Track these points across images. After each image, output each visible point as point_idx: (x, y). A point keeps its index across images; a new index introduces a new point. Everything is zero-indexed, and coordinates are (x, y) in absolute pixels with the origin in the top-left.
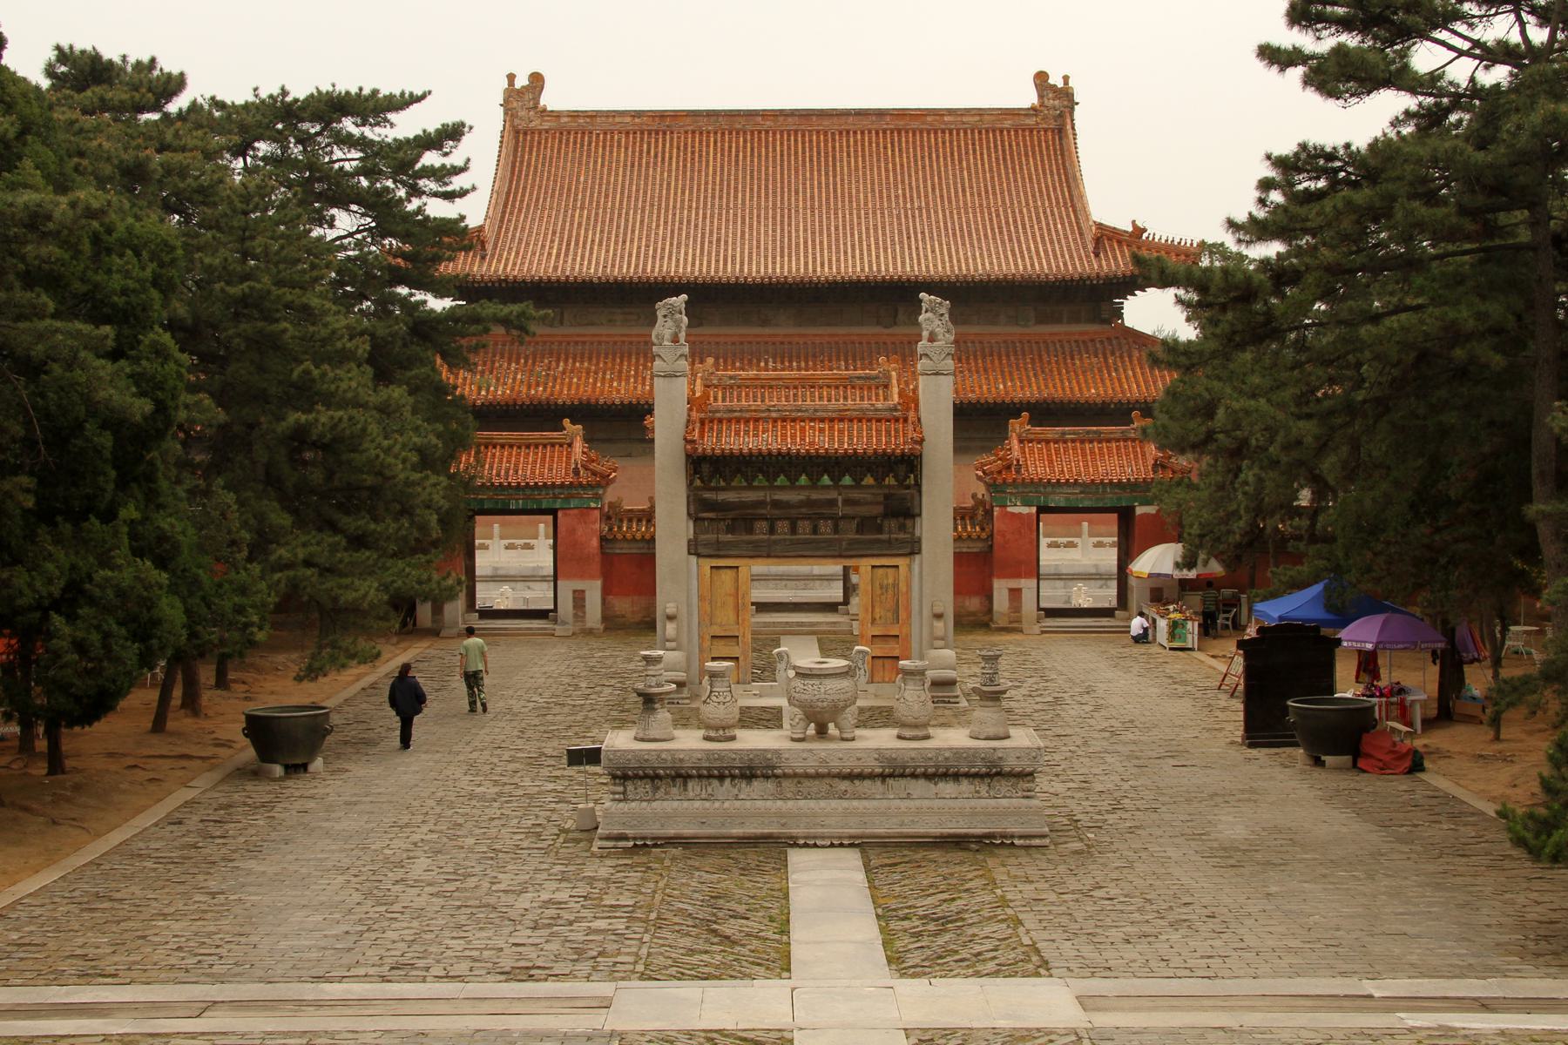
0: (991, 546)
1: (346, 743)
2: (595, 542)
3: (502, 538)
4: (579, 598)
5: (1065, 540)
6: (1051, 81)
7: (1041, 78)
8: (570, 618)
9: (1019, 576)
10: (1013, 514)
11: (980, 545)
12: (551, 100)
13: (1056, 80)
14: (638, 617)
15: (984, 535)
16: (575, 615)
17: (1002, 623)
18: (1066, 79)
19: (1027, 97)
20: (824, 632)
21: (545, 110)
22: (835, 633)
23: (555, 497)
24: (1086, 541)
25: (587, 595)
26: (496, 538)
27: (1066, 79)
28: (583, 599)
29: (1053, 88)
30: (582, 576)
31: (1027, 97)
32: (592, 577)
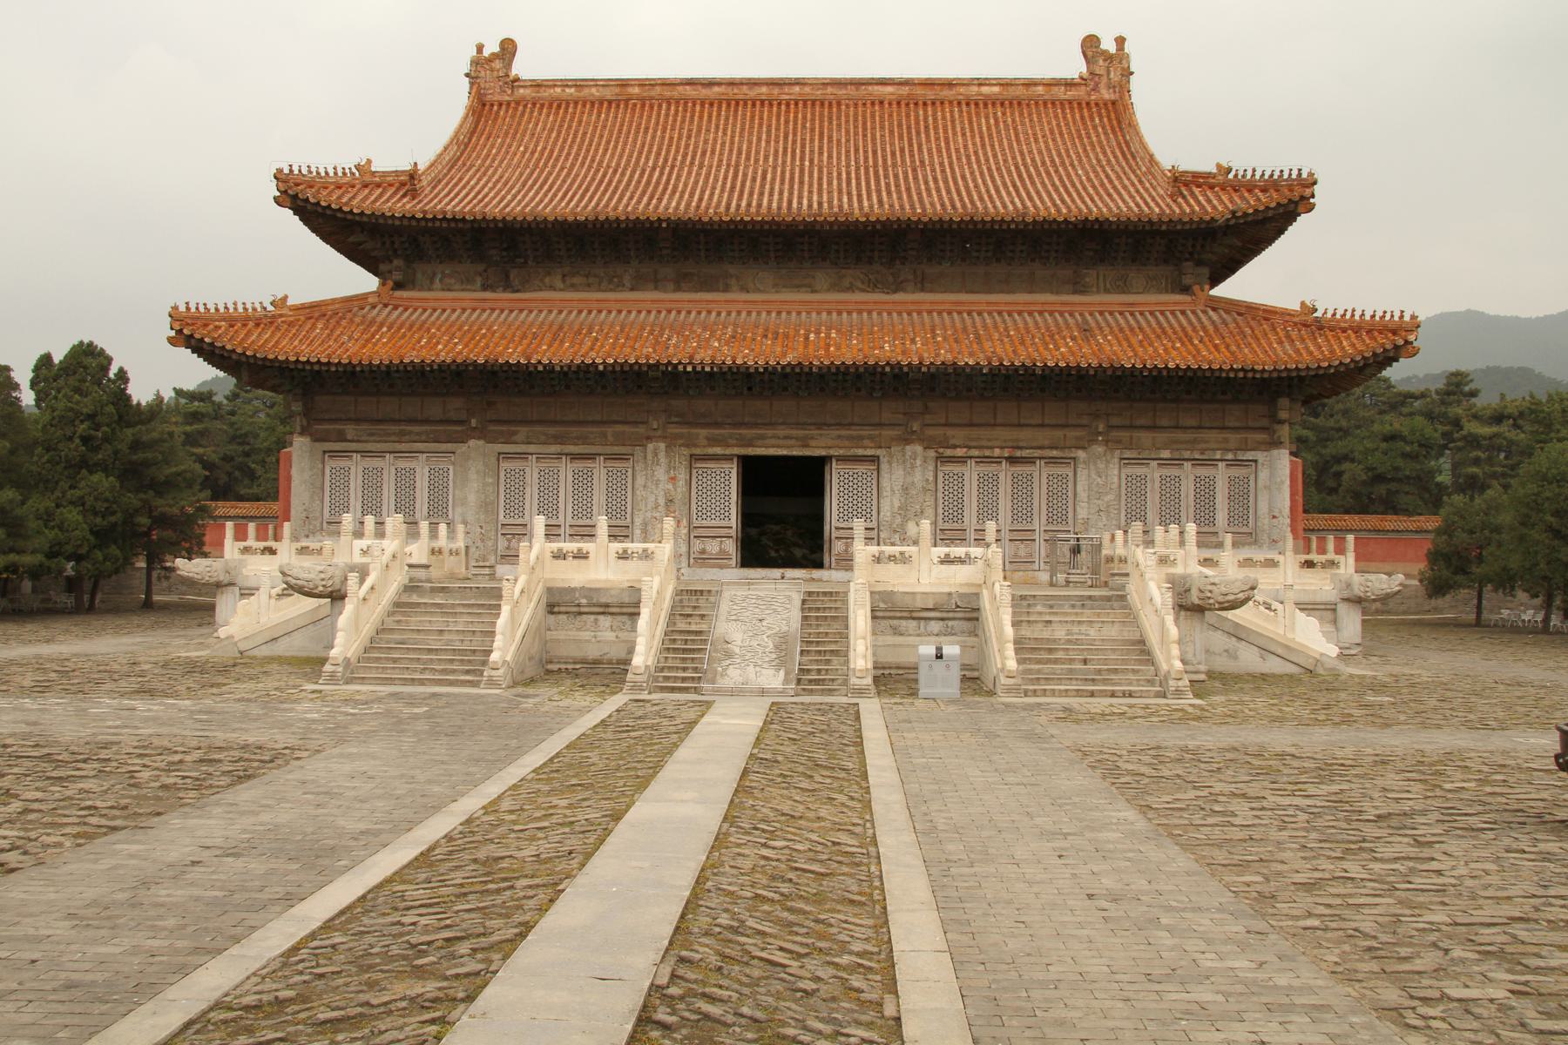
1: (442, 762)
7: (1090, 45)
12: (525, 67)
13: (1109, 45)
18: (1120, 41)
19: (1073, 66)
21: (517, 80)
24: (647, 655)
26: (286, 541)
27: (1120, 41)
31: (1073, 66)
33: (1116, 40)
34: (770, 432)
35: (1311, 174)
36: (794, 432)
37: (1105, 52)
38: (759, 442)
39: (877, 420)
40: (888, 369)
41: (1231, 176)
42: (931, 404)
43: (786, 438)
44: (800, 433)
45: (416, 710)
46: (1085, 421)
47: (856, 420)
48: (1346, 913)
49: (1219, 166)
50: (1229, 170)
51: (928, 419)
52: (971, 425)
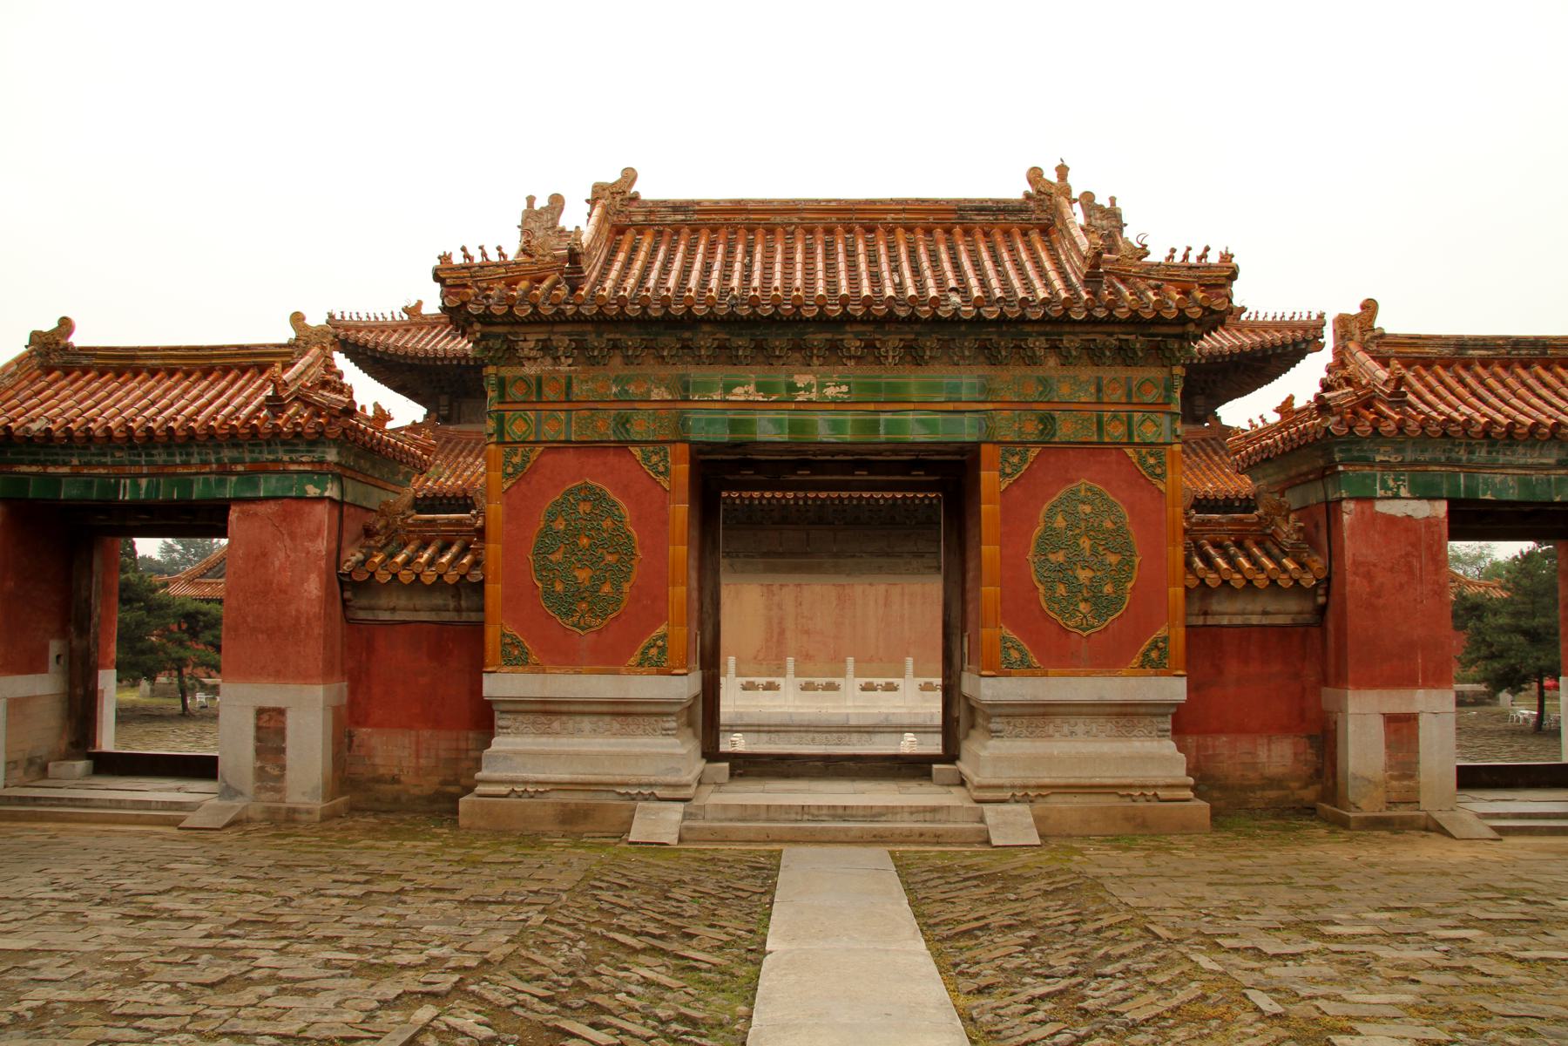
0: (1322, 611)
2: (313, 587)
3: (916, 675)
4: (270, 730)
5: (763, 680)
6: (1098, 201)
8: (248, 783)
9: (1407, 680)
10: (1391, 520)
11: (1293, 605)
13: (1102, 200)
14: (430, 785)
15: (1308, 580)
16: (260, 773)
17: (1367, 804)
18: (1113, 200)
20: (906, 838)
22: (938, 838)
23: (224, 471)
25: (291, 722)
27: (1113, 200)
28: (281, 732)
29: (1100, 208)
30: (280, 673)
32: (304, 677)
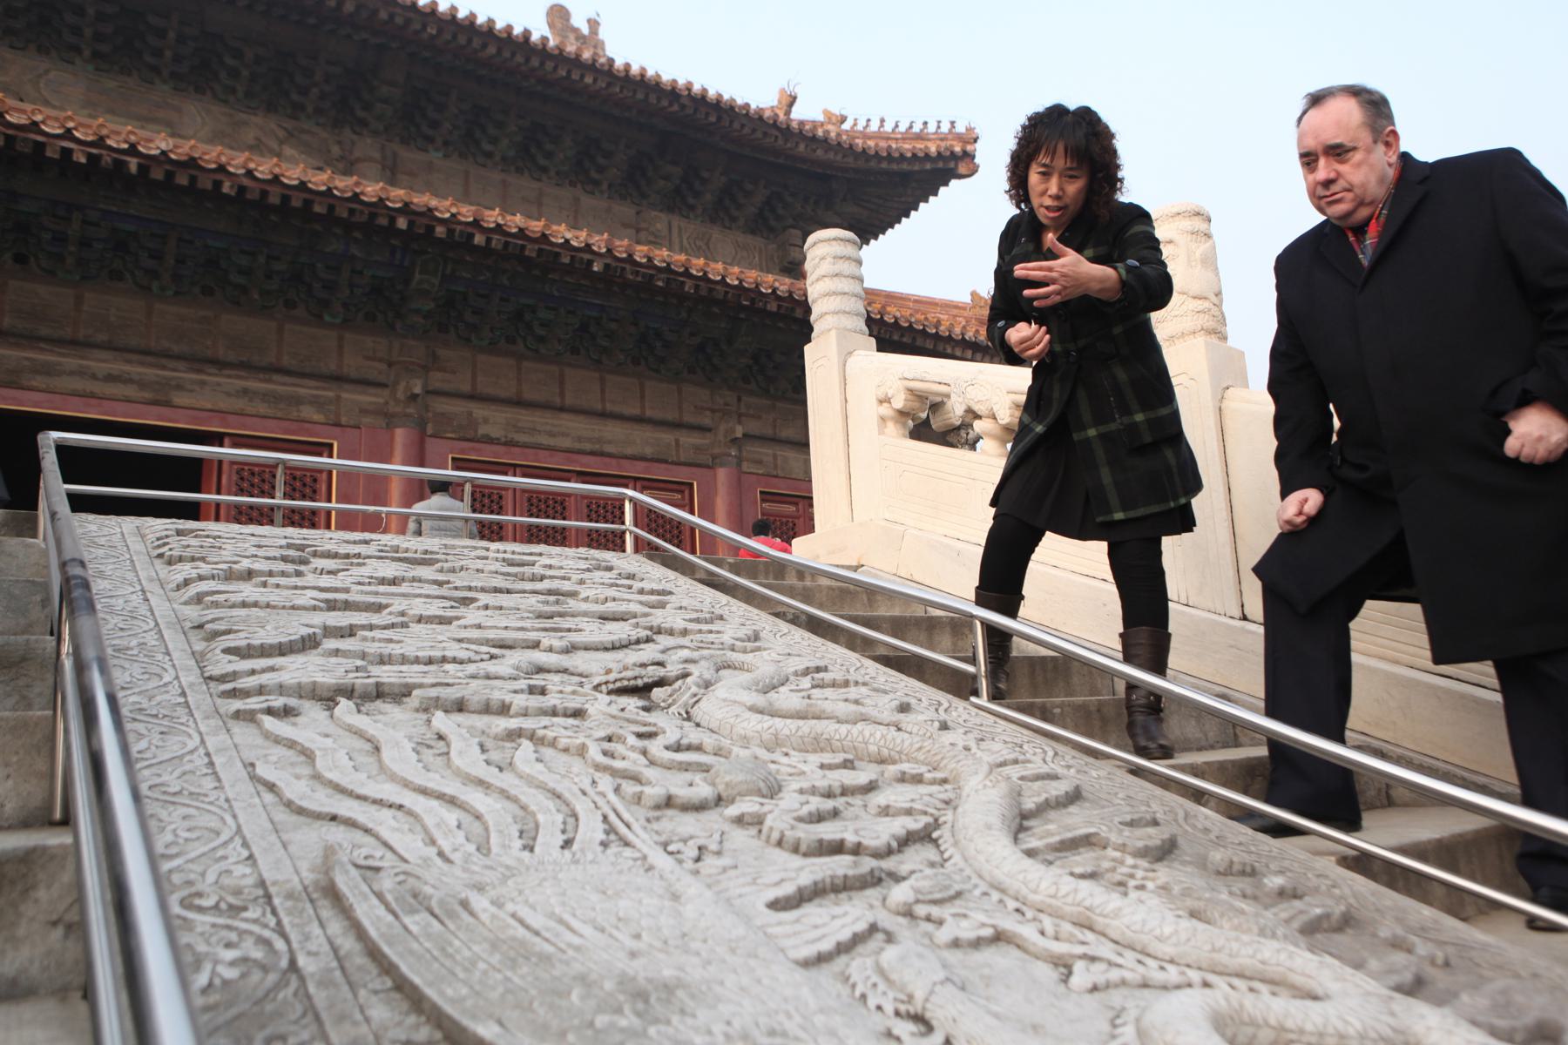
33: (589, 21)
34: (71, 362)
35: (970, 130)
36: (135, 370)
37: (576, 30)
38: (39, 381)
39: (332, 366)
40: (402, 223)
41: (846, 126)
42: (441, 352)
43: (111, 378)
44: (151, 373)
45: (302, 391)
46: (706, 421)
47: (286, 361)
48: (254, 551)
49: (826, 112)
50: (843, 119)
51: (437, 380)
52: (519, 403)
